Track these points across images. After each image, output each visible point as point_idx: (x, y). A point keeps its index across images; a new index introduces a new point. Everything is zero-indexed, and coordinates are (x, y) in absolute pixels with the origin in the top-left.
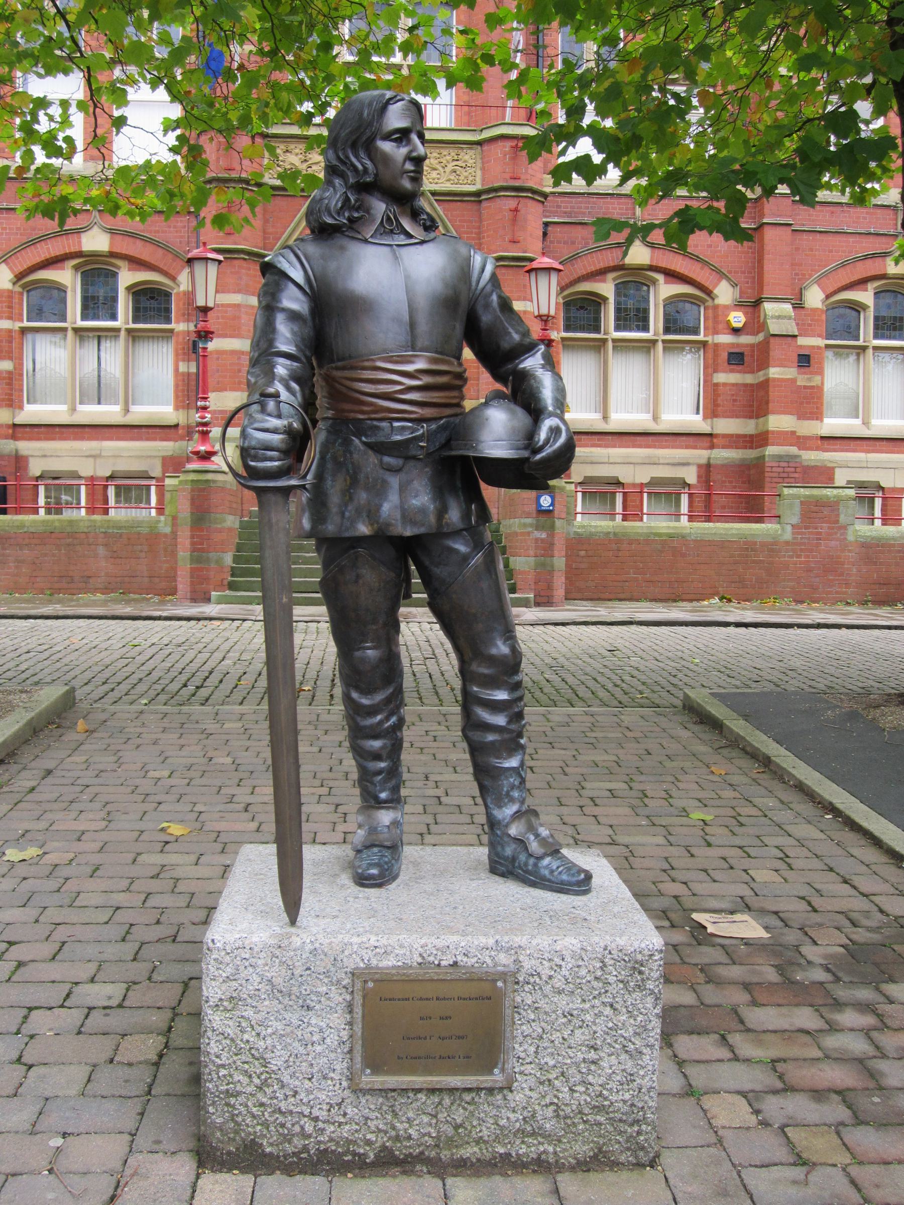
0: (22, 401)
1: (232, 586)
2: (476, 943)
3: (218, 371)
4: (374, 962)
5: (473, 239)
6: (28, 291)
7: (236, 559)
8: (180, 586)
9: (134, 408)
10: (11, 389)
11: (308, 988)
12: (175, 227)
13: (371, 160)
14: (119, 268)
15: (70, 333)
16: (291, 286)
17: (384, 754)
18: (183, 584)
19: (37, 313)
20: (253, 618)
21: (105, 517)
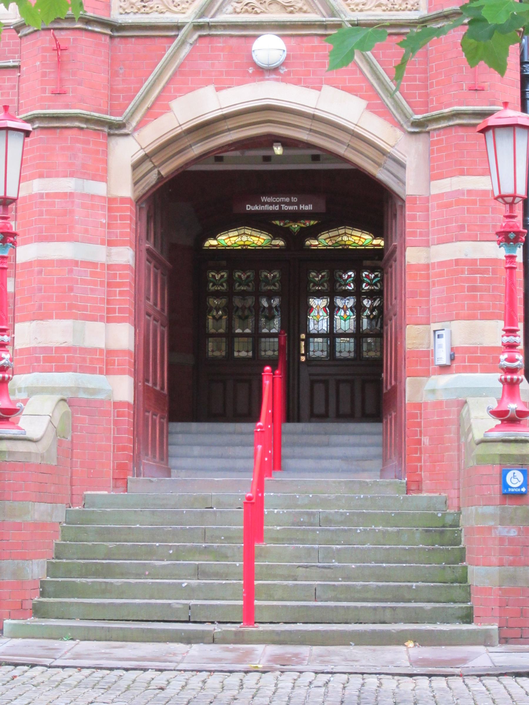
1: (39, 611)
3: (40, 290)
5: (417, 87)
20: (48, 662)
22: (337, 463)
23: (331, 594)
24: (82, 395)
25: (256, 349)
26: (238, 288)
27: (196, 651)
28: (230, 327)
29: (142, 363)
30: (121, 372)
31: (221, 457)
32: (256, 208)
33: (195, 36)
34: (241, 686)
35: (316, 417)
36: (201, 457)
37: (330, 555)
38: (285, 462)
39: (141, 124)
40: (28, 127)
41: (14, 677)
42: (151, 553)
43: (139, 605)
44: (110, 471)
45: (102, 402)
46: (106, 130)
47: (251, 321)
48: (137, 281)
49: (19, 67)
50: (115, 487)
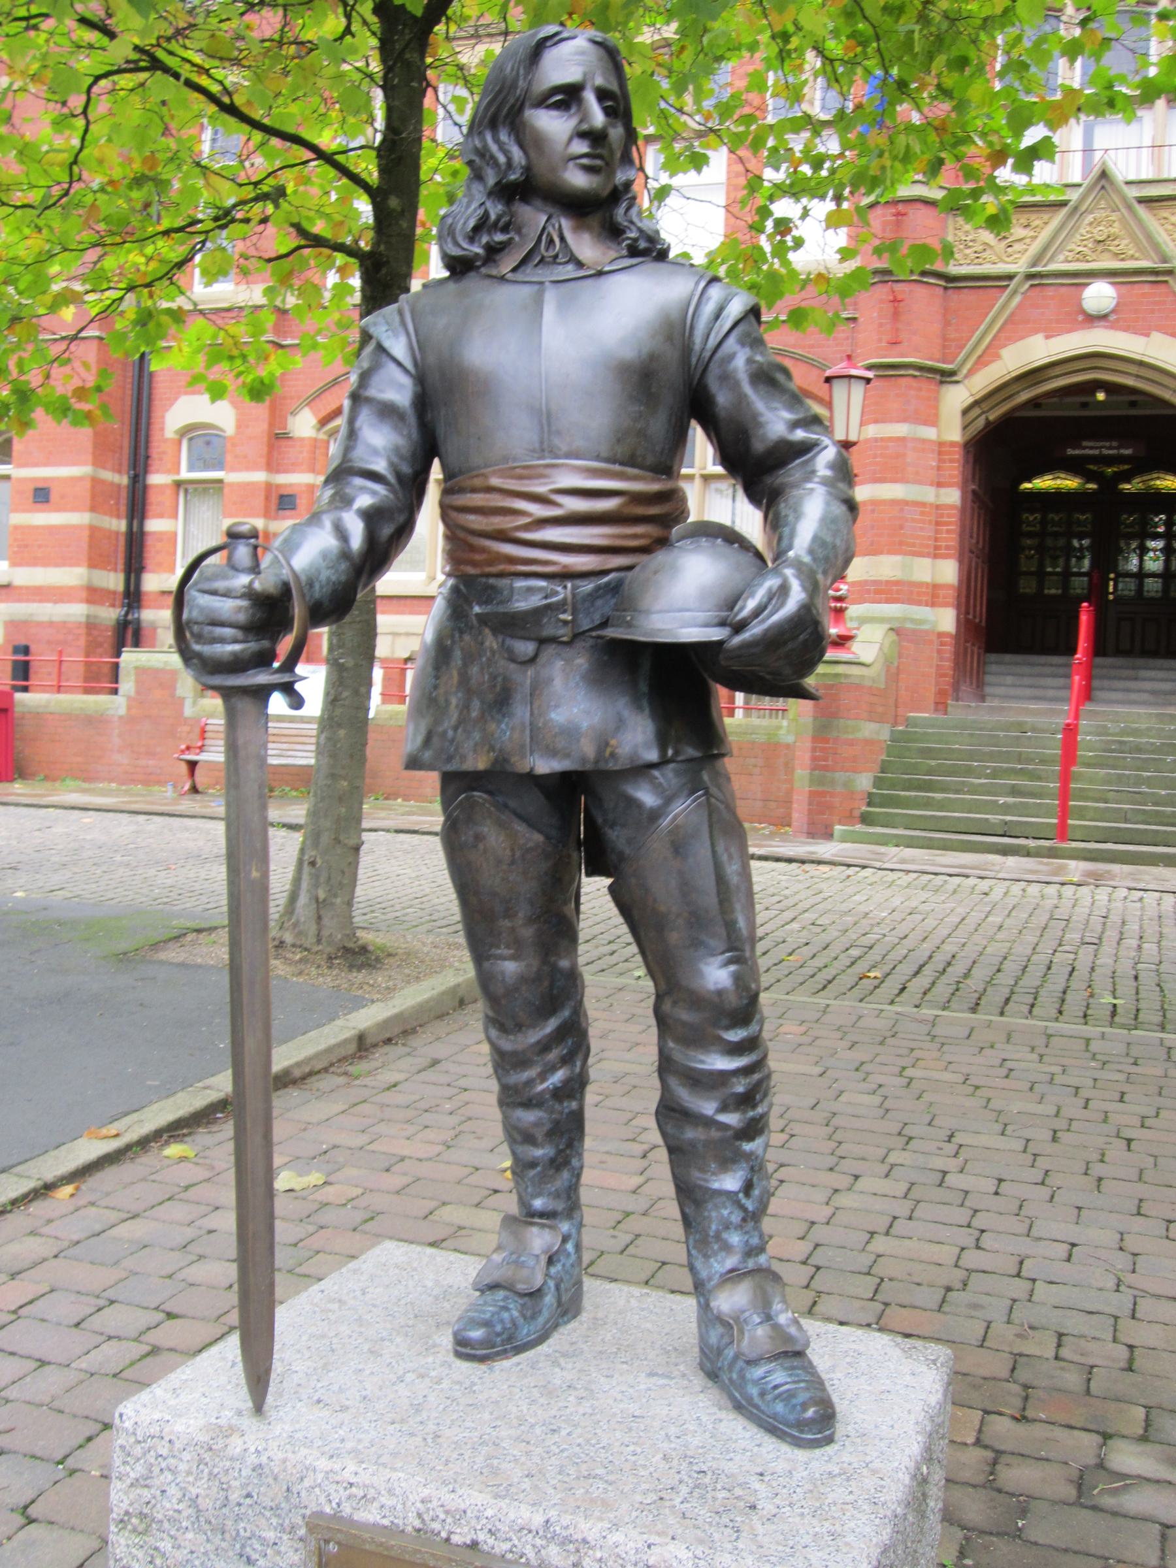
1: (866, 819)
2: (512, 1516)
3: (872, 527)
4: (347, 1510)
7: (878, 782)
8: (795, 815)
11: (248, 1527)
12: (835, 339)
13: (522, 146)
16: (392, 367)
17: (539, 1134)
18: (799, 815)
20: (878, 864)
22: (1145, 696)
23: (1141, 818)
24: (909, 625)
25: (1066, 585)
26: (1050, 529)
27: (1012, 862)
28: (1041, 565)
29: (965, 599)
30: (945, 605)
31: (1031, 686)
32: (1077, 452)
33: (1027, 286)
34: (1060, 896)
35: (1119, 652)
36: (1013, 686)
37: (1140, 781)
38: (1097, 694)
39: (971, 372)
42: (969, 772)
43: (959, 818)
44: (930, 696)
45: (926, 632)
46: (938, 377)
47: (1061, 561)
48: (962, 520)
50: (936, 710)
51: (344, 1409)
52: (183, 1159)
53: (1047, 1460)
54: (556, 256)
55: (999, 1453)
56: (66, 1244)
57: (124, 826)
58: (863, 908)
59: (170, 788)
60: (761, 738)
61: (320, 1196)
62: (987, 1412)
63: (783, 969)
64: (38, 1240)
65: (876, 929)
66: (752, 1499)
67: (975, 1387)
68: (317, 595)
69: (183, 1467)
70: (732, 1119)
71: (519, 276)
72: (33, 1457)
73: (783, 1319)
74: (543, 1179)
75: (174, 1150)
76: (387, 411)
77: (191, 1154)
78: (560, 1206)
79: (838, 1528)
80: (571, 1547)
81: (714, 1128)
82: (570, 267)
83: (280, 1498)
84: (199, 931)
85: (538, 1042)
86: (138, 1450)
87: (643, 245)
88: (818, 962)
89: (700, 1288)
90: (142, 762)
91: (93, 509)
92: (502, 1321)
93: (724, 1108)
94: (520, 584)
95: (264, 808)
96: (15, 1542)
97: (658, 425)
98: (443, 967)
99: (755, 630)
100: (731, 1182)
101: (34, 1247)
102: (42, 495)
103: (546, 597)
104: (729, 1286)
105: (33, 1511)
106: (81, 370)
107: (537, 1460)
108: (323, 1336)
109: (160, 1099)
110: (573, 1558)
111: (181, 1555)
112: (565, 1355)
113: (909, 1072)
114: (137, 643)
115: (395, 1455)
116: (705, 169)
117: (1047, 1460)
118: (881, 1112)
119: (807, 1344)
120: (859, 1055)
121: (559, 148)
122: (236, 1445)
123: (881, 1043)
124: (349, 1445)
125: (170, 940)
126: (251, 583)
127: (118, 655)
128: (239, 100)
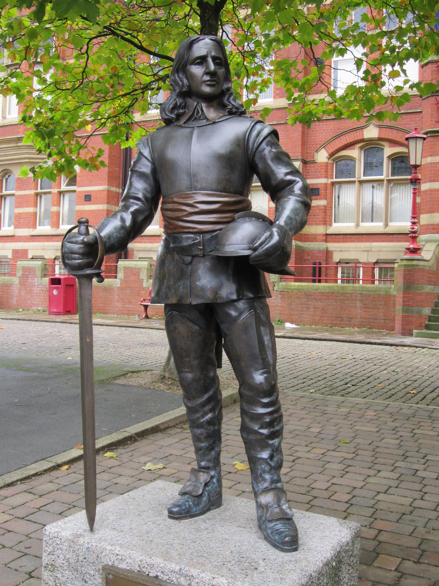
0: (331, 222)
1: (427, 327)
2: (169, 567)
3: (430, 201)
4: (116, 564)
6: (336, 163)
7: (433, 311)
8: (397, 326)
9: (390, 224)
10: (326, 215)
12: (414, 121)
14: (384, 146)
15: (357, 183)
18: (398, 325)
19: (340, 174)
20: (430, 346)
21: (336, 284)
40: (425, 136)
41: (416, 352)
49: (421, 112)
51: (122, 531)
52: (111, 458)
53: (423, 577)
54: (200, 117)
55: (403, 574)
56: (62, 486)
57: (116, 331)
58: (417, 365)
59: (137, 316)
60: (383, 293)
61: (161, 472)
62: (403, 559)
63: (375, 389)
64: (52, 484)
65: (420, 374)
66: (257, 566)
67: (402, 550)
68: (112, 242)
69: (64, 548)
70: (264, 431)
71: (186, 125)
72: (36, 557)
73: (284, 507)
74: (204, 455)
75: (108, 454)
76: (142, 175)
77: (115, 456)
78: (211, 465)
79: (285, 577)
80: (188, 578)
81: (265, 436)
82: (205, 121)
83: (95, 559)
84: (133, 372)
85: (200, 404)
86: (50, 542)
87: (234, 110)
88: (390, 387)
89: (256, 495)
90: (127, 306)
91: (108, 203)
92: (185, 505)
93: (261, 428)
94: (185, 236)
95: (91, 317)
96: (24, 584)
97: (235, 177)
98: (228, 387)
99: (260, 251)
100: (265, 455)
101: (51, 486)
102: (88, 198)
103: (193, 241)
104: (264, 494)
105: (33, 574)
106: (92, 150)
107: (184, 550)
108: (123, 509)
109: (106, 435)
110: (189, 582)
111: (64, 579)
112: (208, 519)
113: (415, 431)
114: (126, 257)
115: (134, 546)
116: (345, 55)
117: (423, 577)
118: (398, 446)
119: (293, 516)
120: (396, 424)
121: (199, 79)
122: (81, 540)
123: (407, 420)
124: (119, 542)
125: (121, 376)
126: (84, 238)
127: (117, 263)
128: (144, 44)
